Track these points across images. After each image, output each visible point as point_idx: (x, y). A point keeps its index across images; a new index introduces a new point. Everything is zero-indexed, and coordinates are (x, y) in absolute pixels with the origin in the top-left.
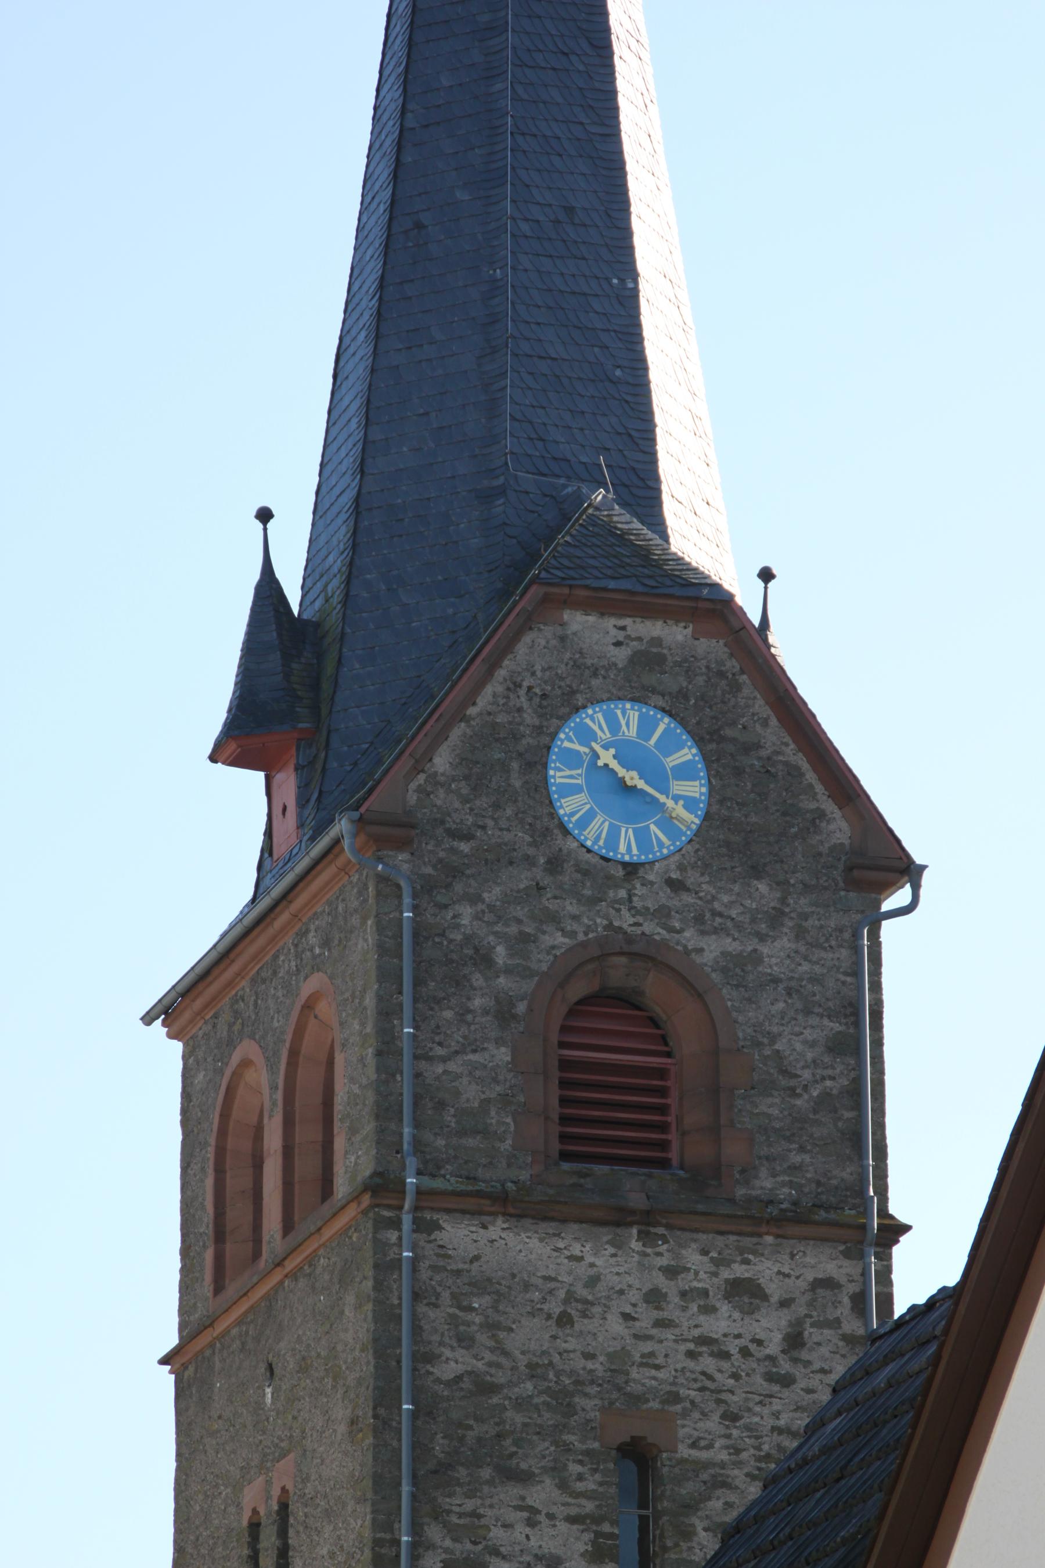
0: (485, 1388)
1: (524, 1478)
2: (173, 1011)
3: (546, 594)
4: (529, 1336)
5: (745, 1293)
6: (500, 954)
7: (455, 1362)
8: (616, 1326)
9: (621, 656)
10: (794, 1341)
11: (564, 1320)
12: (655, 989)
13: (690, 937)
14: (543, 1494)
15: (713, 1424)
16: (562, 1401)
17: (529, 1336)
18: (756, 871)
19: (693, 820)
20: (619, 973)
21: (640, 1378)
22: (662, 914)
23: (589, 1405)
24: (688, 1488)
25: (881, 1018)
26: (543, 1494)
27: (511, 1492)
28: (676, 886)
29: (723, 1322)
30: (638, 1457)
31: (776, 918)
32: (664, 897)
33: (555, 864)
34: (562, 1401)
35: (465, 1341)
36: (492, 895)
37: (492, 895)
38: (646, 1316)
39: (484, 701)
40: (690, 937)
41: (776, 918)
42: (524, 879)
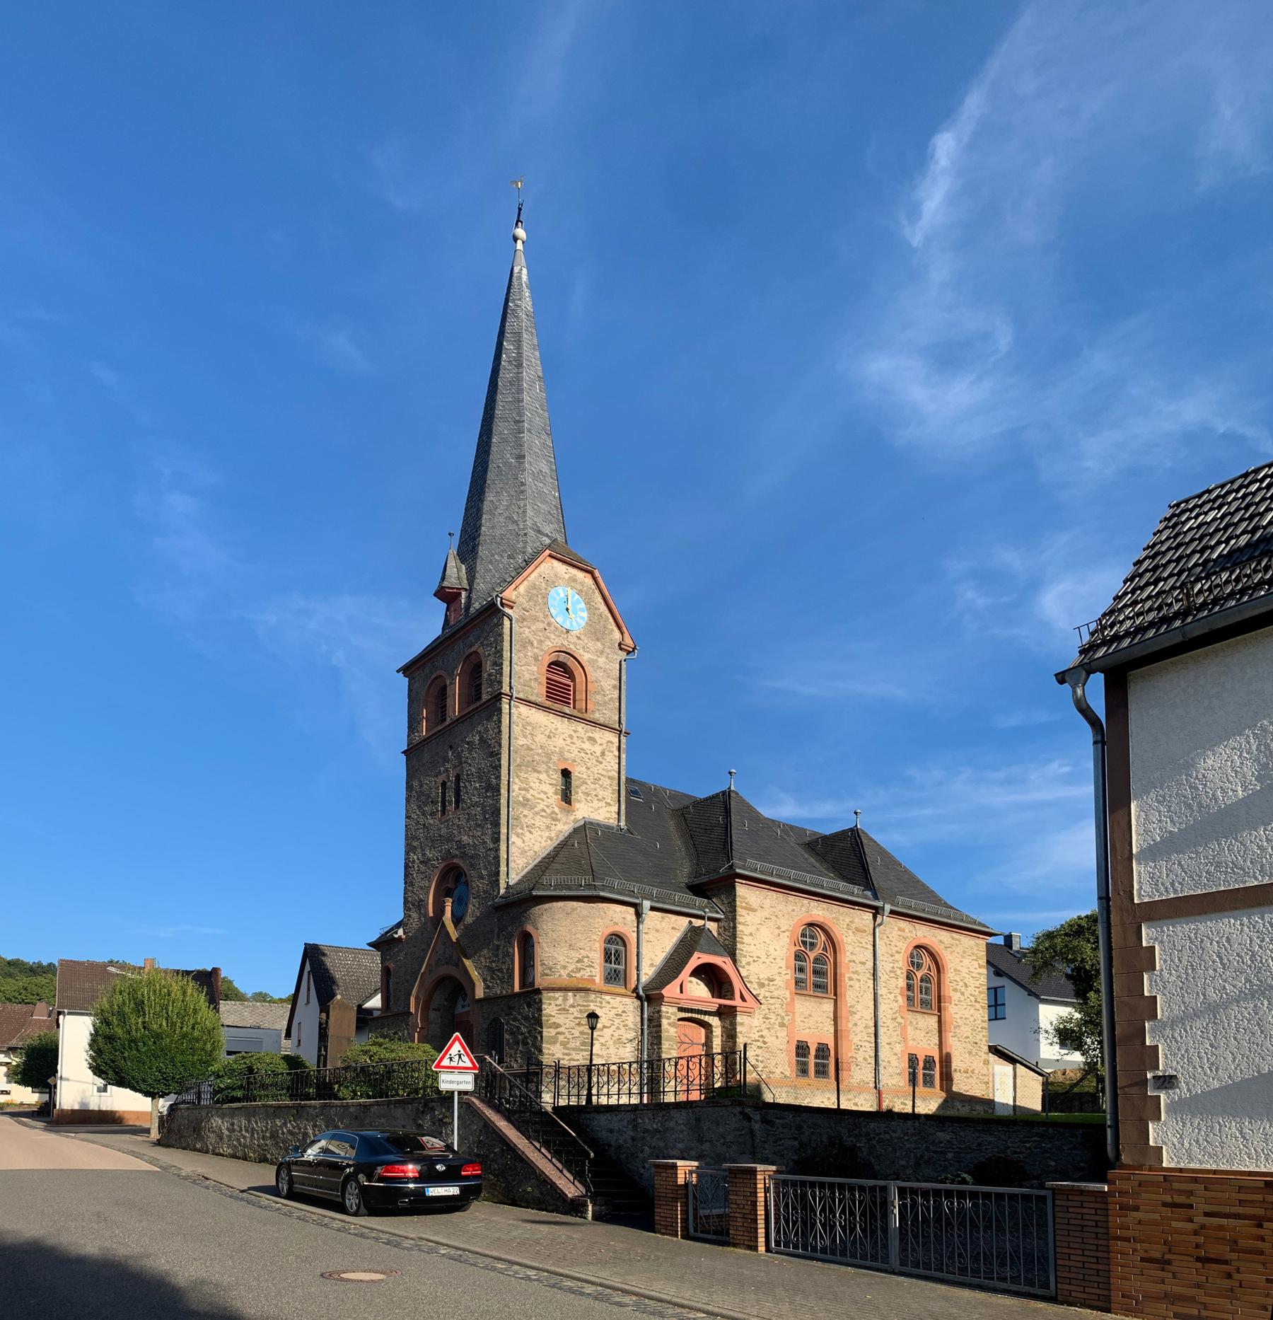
0: (529, 749)
1: (539, 772)
2: (407, 670)
3: (480, 698)
4: (540, 739)
5: (591, 739)
6: (535, 643)
7: (522, 741)
8: (561, 741)
9: (567, 576)
10: (603, 754)
11: (549, 737)
12: (571, 663)
13: (581, 651)
14: (543, 777)
15: (584, 769)
16: (549, 756)
17: (540, 739)
18: (598, 640)
19: (583, 624)
20: (563, 658)
21: (567, 755)
22: (575, 644)
23: (555, 758)
24: (577, 783)
25: (470, 499)
26: (543, 777)
27: (536, 775)
28: (579, 638)
29: (587, 746)
30: (566, 774)
31: (602, 652)
32: (575, 640)
33: (549, 624)
34: (549, 756)
35: (525, 736)
36: (533, 628)
37: (533, 628)
38: (569, 741)
39: (532, 576)
40: (581, 651)
41: (602, 652)
42: (542, 626)
